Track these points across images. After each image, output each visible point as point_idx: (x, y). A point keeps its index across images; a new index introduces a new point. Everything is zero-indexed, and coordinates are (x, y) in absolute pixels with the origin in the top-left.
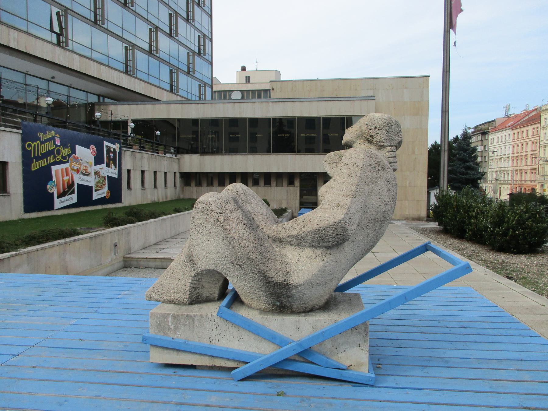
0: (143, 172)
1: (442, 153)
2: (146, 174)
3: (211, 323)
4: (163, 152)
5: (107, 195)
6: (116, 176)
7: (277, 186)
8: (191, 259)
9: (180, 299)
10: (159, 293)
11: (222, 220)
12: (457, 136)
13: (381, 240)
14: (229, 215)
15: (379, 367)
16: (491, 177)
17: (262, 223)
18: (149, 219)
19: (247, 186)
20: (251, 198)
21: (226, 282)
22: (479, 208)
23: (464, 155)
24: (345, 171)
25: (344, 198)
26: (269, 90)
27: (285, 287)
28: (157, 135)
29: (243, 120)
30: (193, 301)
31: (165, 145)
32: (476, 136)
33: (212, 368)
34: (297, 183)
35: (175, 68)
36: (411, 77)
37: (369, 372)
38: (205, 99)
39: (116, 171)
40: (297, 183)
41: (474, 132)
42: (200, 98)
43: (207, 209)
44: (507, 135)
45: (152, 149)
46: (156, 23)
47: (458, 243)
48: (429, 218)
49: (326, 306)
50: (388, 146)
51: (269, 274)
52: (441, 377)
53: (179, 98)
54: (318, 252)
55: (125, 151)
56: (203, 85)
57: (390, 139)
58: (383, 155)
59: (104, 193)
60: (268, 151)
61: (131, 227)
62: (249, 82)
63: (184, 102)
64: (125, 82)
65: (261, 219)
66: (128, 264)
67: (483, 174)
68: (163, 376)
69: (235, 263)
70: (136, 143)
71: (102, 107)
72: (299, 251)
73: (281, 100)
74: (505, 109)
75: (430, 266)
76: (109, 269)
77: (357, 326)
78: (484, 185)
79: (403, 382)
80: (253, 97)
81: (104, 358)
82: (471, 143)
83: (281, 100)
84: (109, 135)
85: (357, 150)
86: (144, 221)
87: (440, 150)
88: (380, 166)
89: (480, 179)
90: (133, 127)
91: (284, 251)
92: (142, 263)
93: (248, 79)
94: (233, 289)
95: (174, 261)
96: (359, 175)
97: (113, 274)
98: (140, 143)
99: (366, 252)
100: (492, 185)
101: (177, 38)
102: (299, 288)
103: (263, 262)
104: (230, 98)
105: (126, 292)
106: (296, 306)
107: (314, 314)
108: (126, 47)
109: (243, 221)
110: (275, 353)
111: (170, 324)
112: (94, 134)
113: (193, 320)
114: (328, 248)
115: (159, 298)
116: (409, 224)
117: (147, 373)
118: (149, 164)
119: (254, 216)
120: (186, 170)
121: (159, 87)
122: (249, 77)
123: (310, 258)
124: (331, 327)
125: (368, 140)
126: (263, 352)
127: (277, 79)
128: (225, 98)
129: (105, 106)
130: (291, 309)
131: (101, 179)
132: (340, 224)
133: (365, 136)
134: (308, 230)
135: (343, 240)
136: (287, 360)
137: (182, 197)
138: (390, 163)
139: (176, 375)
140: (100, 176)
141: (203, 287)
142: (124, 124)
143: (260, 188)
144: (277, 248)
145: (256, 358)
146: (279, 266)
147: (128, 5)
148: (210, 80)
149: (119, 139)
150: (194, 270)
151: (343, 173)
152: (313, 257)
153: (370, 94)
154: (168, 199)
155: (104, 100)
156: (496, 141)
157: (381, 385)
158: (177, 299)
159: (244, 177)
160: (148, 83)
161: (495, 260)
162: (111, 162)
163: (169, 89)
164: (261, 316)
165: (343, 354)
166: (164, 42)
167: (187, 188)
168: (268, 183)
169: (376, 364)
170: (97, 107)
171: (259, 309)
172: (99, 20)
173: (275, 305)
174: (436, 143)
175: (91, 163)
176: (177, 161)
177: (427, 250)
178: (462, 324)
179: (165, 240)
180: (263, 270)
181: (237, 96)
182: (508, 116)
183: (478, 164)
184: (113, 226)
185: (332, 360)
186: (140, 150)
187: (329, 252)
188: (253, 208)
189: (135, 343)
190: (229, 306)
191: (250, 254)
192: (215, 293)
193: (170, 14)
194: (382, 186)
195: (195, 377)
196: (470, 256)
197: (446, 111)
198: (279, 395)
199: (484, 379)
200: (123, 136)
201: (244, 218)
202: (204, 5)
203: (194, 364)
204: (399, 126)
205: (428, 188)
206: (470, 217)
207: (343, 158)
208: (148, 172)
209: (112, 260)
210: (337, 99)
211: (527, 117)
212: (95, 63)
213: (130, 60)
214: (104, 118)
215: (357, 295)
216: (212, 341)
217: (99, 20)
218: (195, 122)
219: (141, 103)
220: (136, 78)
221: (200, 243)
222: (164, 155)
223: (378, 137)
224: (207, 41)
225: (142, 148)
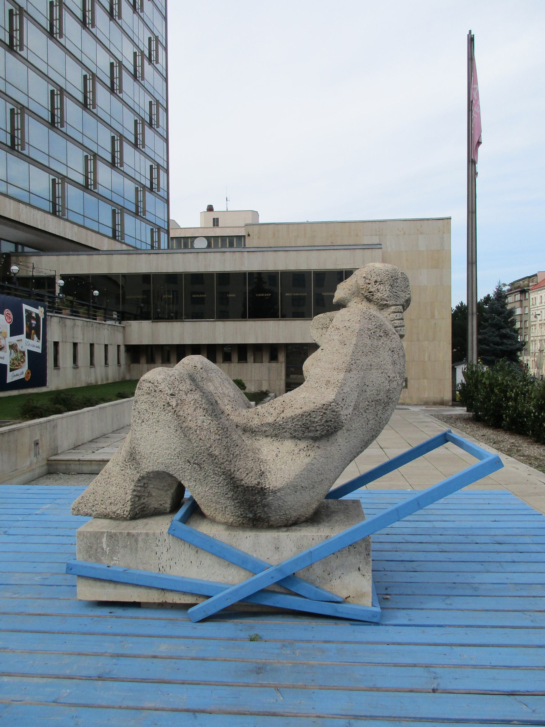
0: (75, 345)
1: (470, 317)
2: (80, 348)
3: (160, 544)
4: (102, 318)
5: (27, 377)
6: (39, 351)
7: (255, 362)
8: (133, 457)
10: (90, 505)
11: (174, 404)
12: (489, 295)
13: (386, 427)
14: (184, 397)
15: (387, 599)
16: (534, 347)
17: (228, 407)
18: (83, 408)
20: (213, 375)
21: (181, 489)
22: (518, 387)
23: (498, 320)
24: (337, 337)
25: (335, 373)
26: (244, 236)
27: (259, 492)
28: (92, 296)
29: (210, 275)
30: (136, 514)
31: (105, 309)
32: (513, 295)
33: (162, 606)
34: (282, 358)
35: (120, 208)
36: (428, 220)
37: (373, 606)
38: (159, 248)
39: (40, 344)
40: (282, 358)
41: (511, 290)
42: (152, 247)
43: (154, 390)
45: (88, 314)
46: (94, 148)
47: (493, 434)
48: (455, 402)
49: (315, 518)
50: (392, 305)
51: (237, 475)
52: (468, 610)
53: (124, 247)
54: (303, 444)
55: (51, 316)
56: (156, 229)
57: (394, 295)
58: (386, 317)
59: (22, 373)
60: (243, 316)
61: (57, 419)
62: (218, 225)
63: (131, 252)
64: (53, 225)
65: (226, 402)
66: (53, 469)
67: (524, 344)
68: (95, 619)
69: (192, 462)
70: (67, 306)
71: (20, 258)
72: (276, 444)
73: (259, 249)
75: (449, 462)
76: (27, 476)
77: (356, 543)
78: (525, 358)
79: (418, 617)
80: (224, 246)
81: (14, 596)
82: (507, 304)
83: (259, 249)
84: (30, 295)
85: (351, 310)
86: (76, 410)
87: (467, 313)
88: (382, 331)
89: (520, 350)
90: (62, 285)
91: (257, 444)
92: (73, 467)
93: (216, 222)
94: (191, 498)
95: (110, 461)
96: (354, 342)
97: (33, 482)
98: (72, 307)
99: (366, 444)
100: (536, 358)
101: (122, 168)
102: (278, 494)
103: (229, 459)
104: (192, 247)
105: (48, 506)
106: (274, 518)
107: (299, 528)
108: (54, 180)
109: (202, 405)
110: (248, 581)
111: (105, 546)
112: (9, 294)
113: (136, 541)
114: (315, 439)
115: (90, 511)
116: (428, 411)
117: (73, 615)
118: (83, 334)
119: (217, 399)
120: (134, 342)
121: (98, 233)
122: (218, 219)
123: (292, 453)
124: (321, 545)
125: (366, 297)
126: (229, 581)
127: (255, 222)
128: (186, 246)
129: (24, 257)
130: (268, 522)
131: (19, 355)
132: (330, 408)
133: (363, 292)
134: (289, 415)
135: (335, 428)
136: (263, 591)
137: (128, 378)
138: (396, 327)
139: (112, 617)
140: (17, 351)
141: (150, 495)
142: (51, 280)
143: (232, 364)
144: (248, 441)
145: (222, 589)
146: (250, 464)
147: (56, 125)
148: (166, 224)
149: (43, 301)
150: (138, 472)
151: (334, 342)
152: (296, 452)
153: (375, 240)
154: (110, 381)
155: (23, 249)
156: (538, 301)
157: (387, 623)
158: (114, 513)
159: (212, 351)
160: (84, 227)
161: (540, 454)
162: (33, 331)
163: (110, 235)
164: (227, 533)
165: (338, 581)
166: (105, 174)
167: (136, 365)
168: (243, 359)
169: (383, 594)
170: (13, 259)
171: (225, 523)
172: (18, 145)
173: (246, 517)
174: (462, 303)
175: (6, 334)
176: (121, 330)
177: (447, 441)
179: (104, 436)
180: (230, 470)
181: (201, 244)
183: (516, 331)
184: (34, 417)
185: (323, 589)
186: (71, 315)
187: (316, 444)
188: (216, 388)
189: (57, 574)
190: (185, 520)
191: (211, 449)
192: (166, 503)
193: (113, 138)
194: (385, 357)
196: (508, 451)
197: (472, 263)
198: (251, 640)
199: (524, 611)
200: (49, 297)
201: (203, 401)
202: (158, 126)
203: (137, 601)
204: (406, 279)
205: (452, 363)
206: (508, 399)
207: (334, 320)
208: (83, 345)
209: (31, 464)
210: (332, 248)
212: (12, 201)
213: (59, 197)
214: (23, 274)
215: (356, 503)
216: (161, 568)
217: (18, 145)
218: (146, 278)
219: (74, 253)
220: (67, 220)
221: (145, 435)
222: (103, 322)
223: (379, 294)
224: (161, 172)
225: (75, 313)
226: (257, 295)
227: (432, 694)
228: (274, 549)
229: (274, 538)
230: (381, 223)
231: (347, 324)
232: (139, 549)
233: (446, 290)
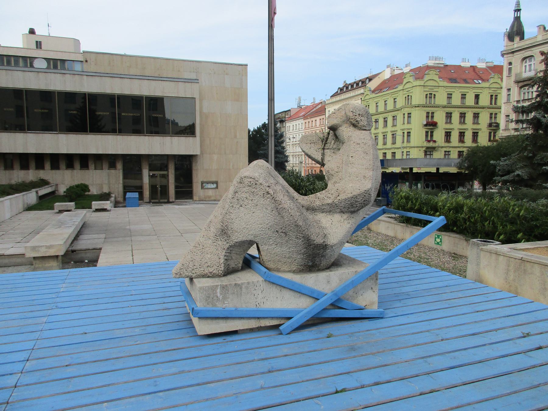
3: (257, 288)
7: (95, 169)
9: (214, 272)
10: (190, 269)
19: (267, 161)
22: (307, 186)
24: (360, 149)
33: (260, 329)
34: (119, 166)
36: (231, 64)
40: (119, 166)
44: (300, 124)
51: (313, 237)
54: (345, 216)
62: (41, 48)
74: (297, 101)
93: (39, 45)
104: (32, 66)
111: (219, 295)
113: (241, 288)
122: (40, 42)
126: (301, 306)
134: (343, 198)
136: (325, 309)
143: (75, 171)
145: (298, 312)
146: (317, 230)
152: (342, 221)
153: (193, 76)
156: (291, 128)
158: (211, 273)
178: (389, 270)
182: (300, 107)
195: (236, 341)
198: (328, 337)
211: (315, 109)
226: (5, 109)
227: (442, 342)
228: (326, 283)
229: (327, 276)
230: (197, 63)
231: (365, 141)
232: (243, 294)
233: (244, 116)
